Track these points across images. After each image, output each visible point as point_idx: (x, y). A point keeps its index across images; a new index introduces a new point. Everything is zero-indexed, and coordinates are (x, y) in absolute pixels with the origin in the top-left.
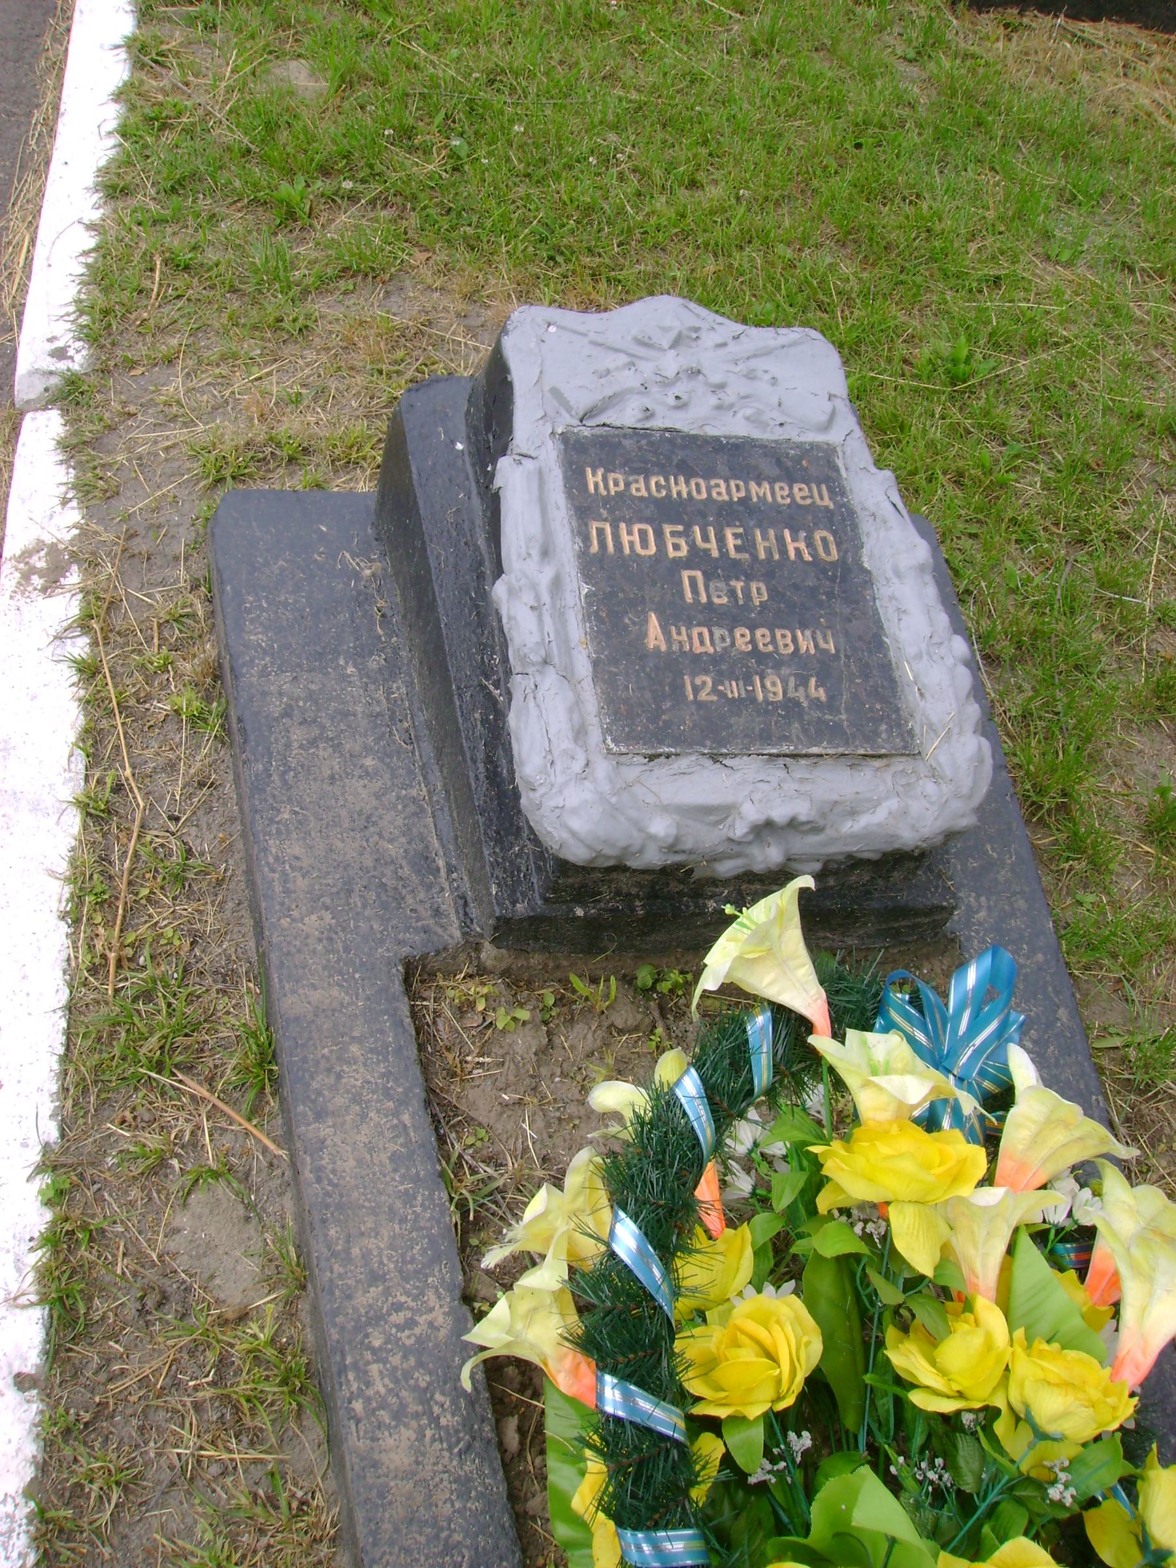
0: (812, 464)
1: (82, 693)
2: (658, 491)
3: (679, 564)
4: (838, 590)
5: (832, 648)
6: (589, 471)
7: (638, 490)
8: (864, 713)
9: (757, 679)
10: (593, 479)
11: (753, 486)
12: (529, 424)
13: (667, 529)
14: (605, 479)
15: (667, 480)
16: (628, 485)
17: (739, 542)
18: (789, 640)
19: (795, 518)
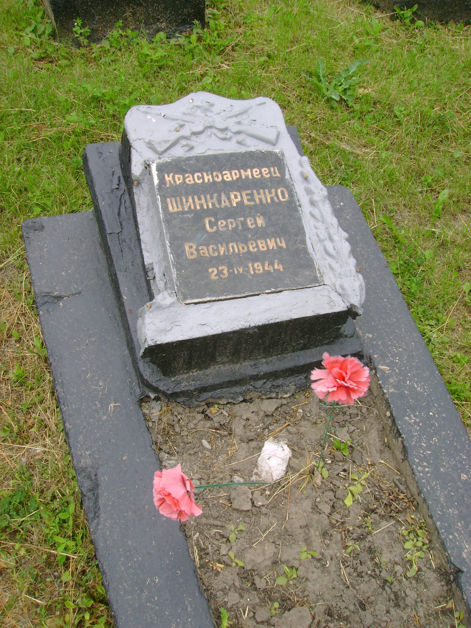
4: (286, 220)
5: (284, 245)
7: (227, 178)
8: (299, 269)
14: (173, 177)
16: (184, 179)
17: (249, 197)
18: (264, 245)
19: (259, 184)
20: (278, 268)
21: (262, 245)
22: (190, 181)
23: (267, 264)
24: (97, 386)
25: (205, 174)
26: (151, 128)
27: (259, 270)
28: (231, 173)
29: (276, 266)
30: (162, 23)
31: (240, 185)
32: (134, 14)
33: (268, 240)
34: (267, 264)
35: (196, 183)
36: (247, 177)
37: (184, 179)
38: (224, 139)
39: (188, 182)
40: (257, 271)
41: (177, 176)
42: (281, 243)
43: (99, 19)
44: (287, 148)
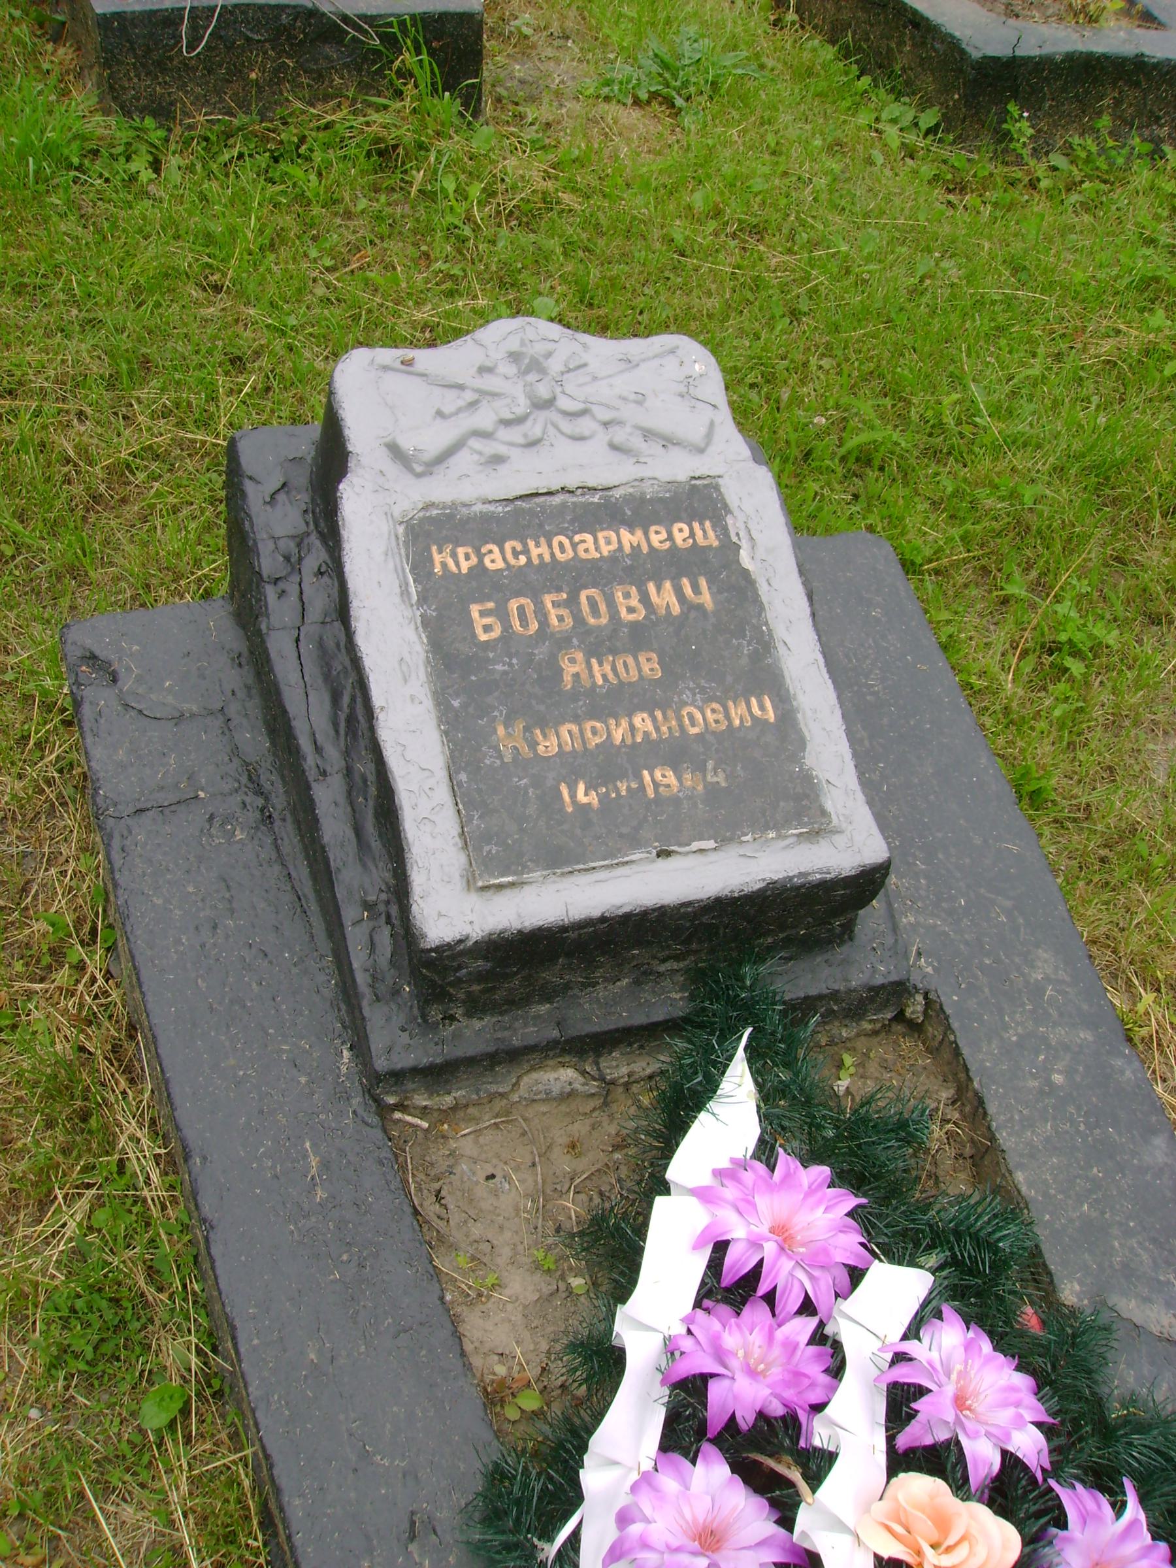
0: (700, 500)
1: (852, 1202)
3: (563, 642)
6: (434, 548)
8: (803, 810)
10: (439, 558)
11: (625, 534)
12: (369, 513)
13: (548, 599)
15: (525, 545)
20: (715, 779)
21: (715, 716)
22: (586, 551)
23: (581, 787)
25: (531, 544)
26: (371, 390)
28: (502, 551)
29: (710, 778)
30: (1162, 126)
31: (637, 570)
32: (1118, 102)
33: (651, 587)
34: (581, 787)
35: (509, 566)
37: (481, 557)
39: (583, 555)
41: (461, 551)
42: (762, 707)
43: (1051, 107)
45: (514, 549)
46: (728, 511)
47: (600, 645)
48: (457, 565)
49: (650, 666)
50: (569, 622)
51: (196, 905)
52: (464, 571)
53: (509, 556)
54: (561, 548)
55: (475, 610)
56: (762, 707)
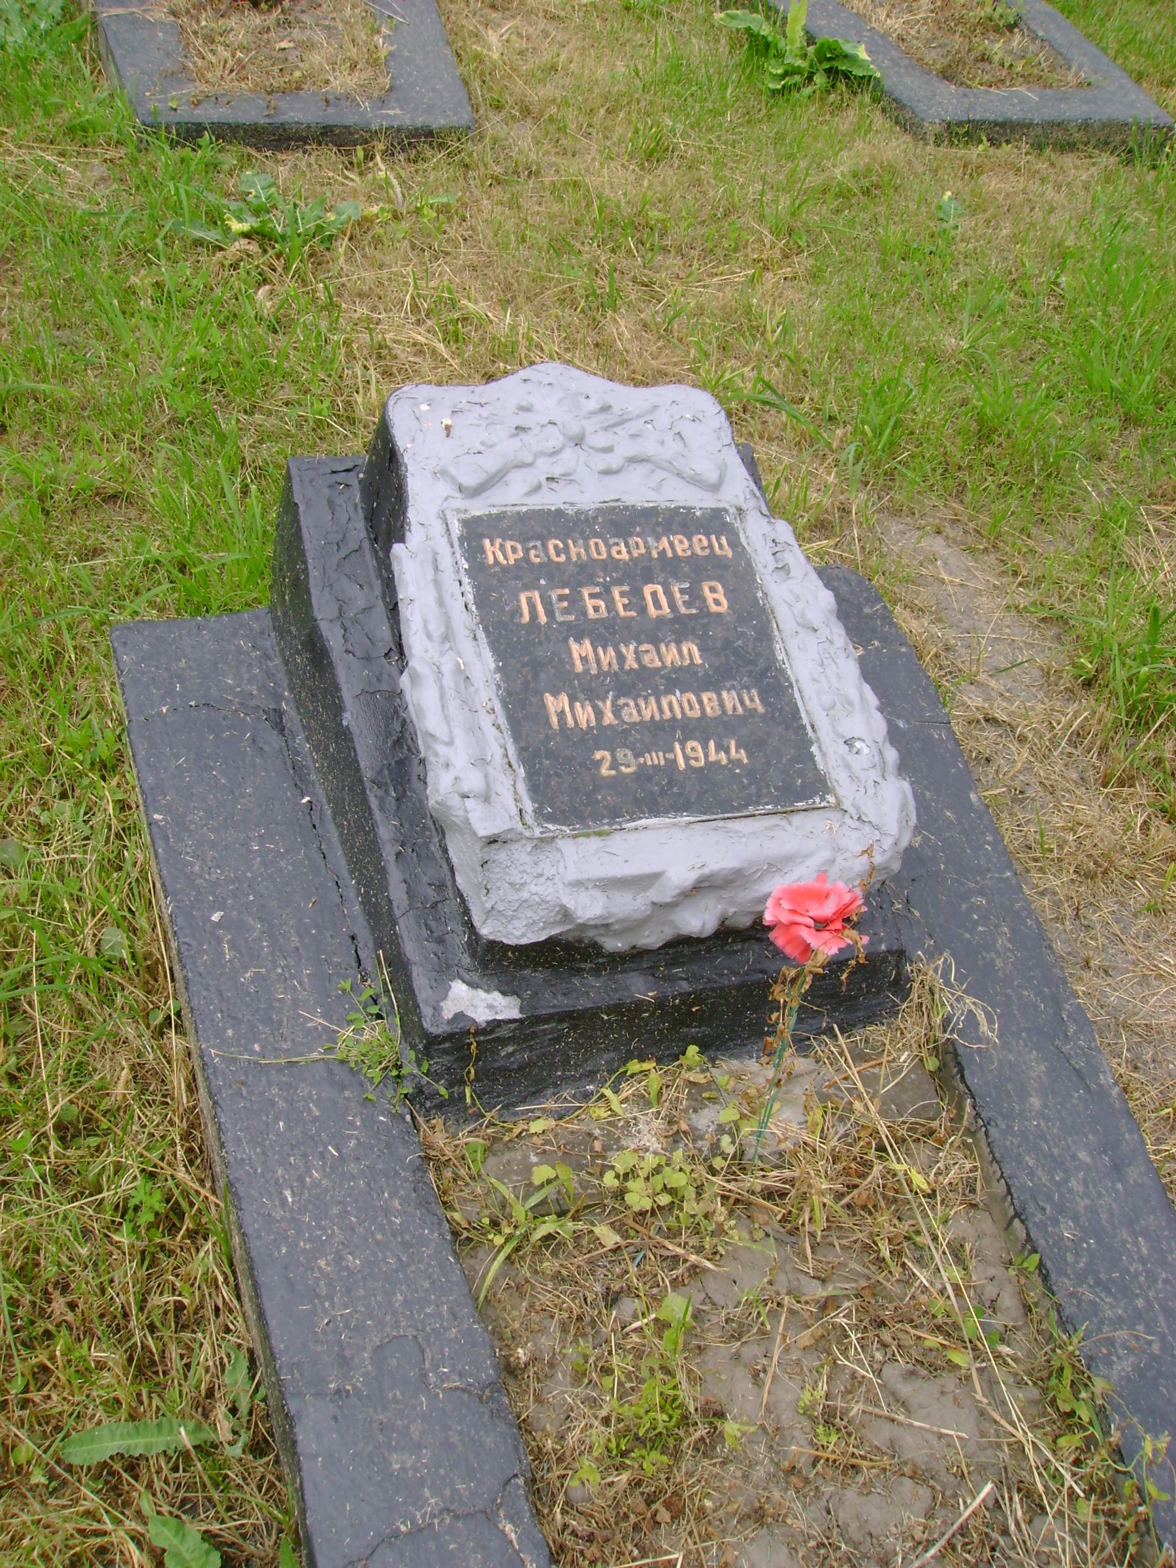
0: (714, 522)
2: (558, 555)
4: (744, 650)
9: (677, 746)
10: (492, 551)
12: (428, 502)
16: (527, 551)
24: (291, 1057)
27: (697, 759)
28: (627, 545)
31: (638, 573)
36: (663, 553)
38: (607, 472)
40: (693, 763)
41: (508, 544)
42: (752, 700)
44: (738, 489)
45: (556, 547)
46: (402, 540)
47: (607, 632)
48: (506, 558)
49: (692, 651)
50: (603, 613)
51: (232, 862)
52: (512, 562)
53: (552, 551)
54: (680, 545)
55: (586, 593)
56: (752, 700)
